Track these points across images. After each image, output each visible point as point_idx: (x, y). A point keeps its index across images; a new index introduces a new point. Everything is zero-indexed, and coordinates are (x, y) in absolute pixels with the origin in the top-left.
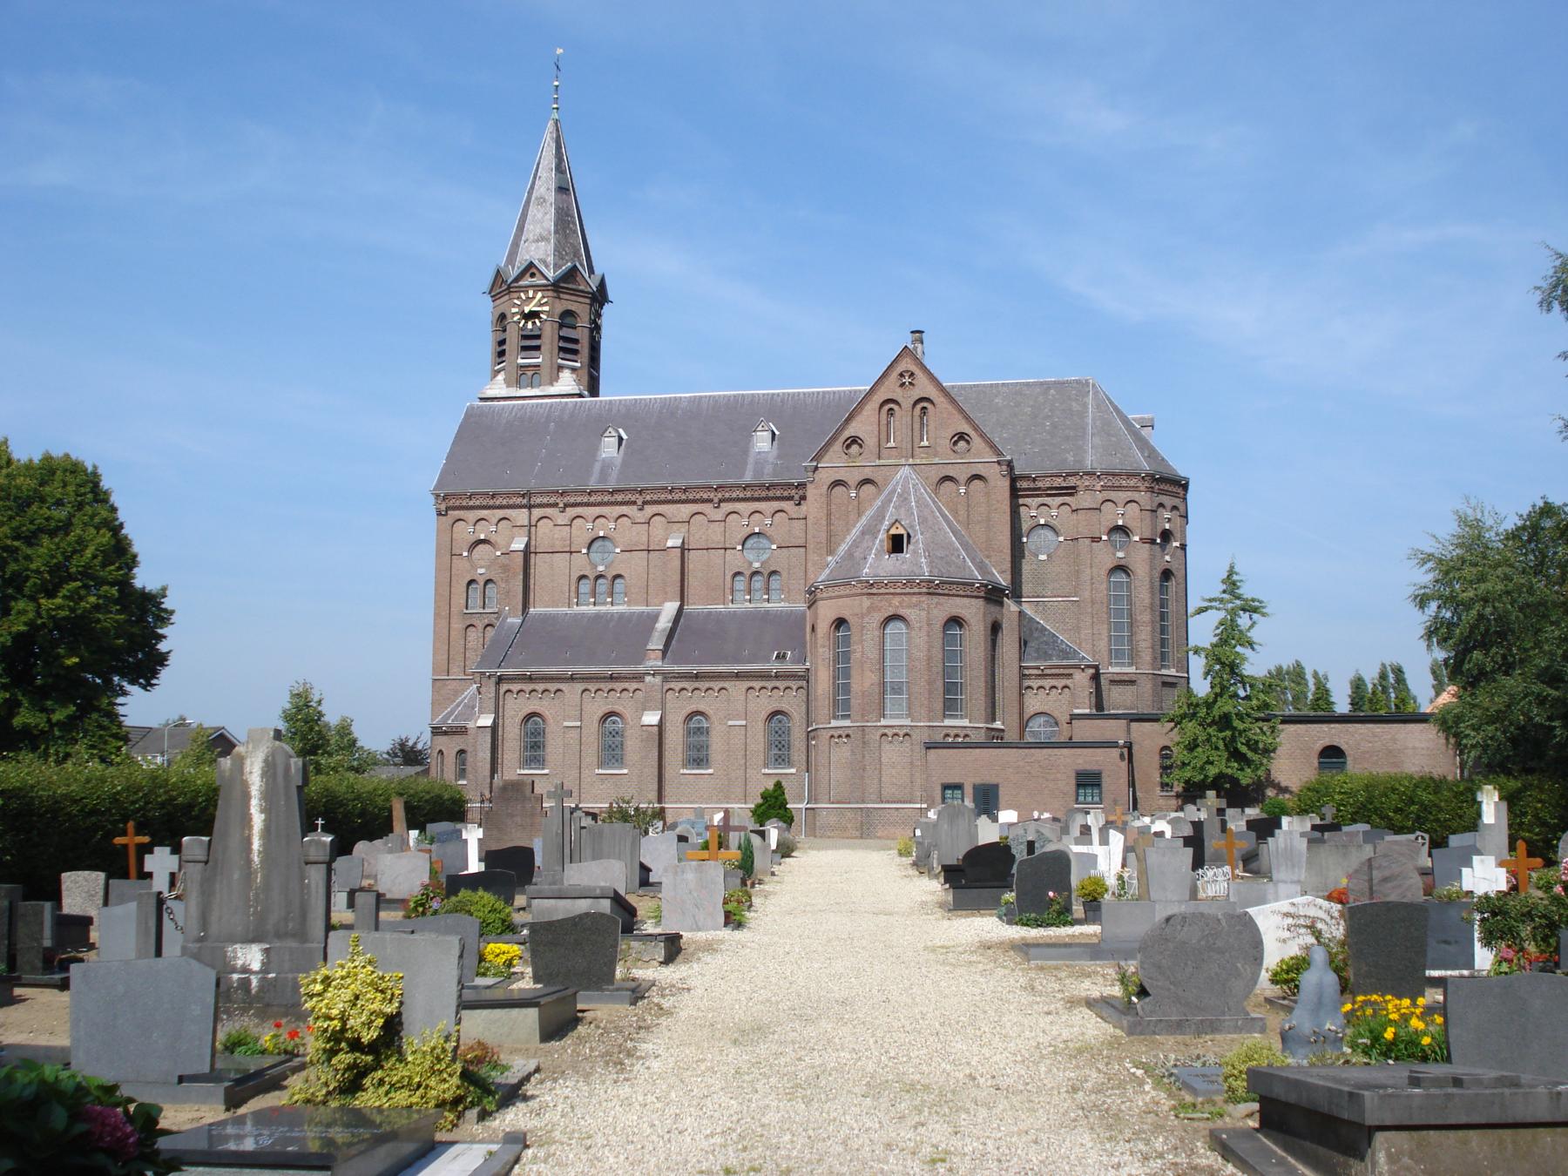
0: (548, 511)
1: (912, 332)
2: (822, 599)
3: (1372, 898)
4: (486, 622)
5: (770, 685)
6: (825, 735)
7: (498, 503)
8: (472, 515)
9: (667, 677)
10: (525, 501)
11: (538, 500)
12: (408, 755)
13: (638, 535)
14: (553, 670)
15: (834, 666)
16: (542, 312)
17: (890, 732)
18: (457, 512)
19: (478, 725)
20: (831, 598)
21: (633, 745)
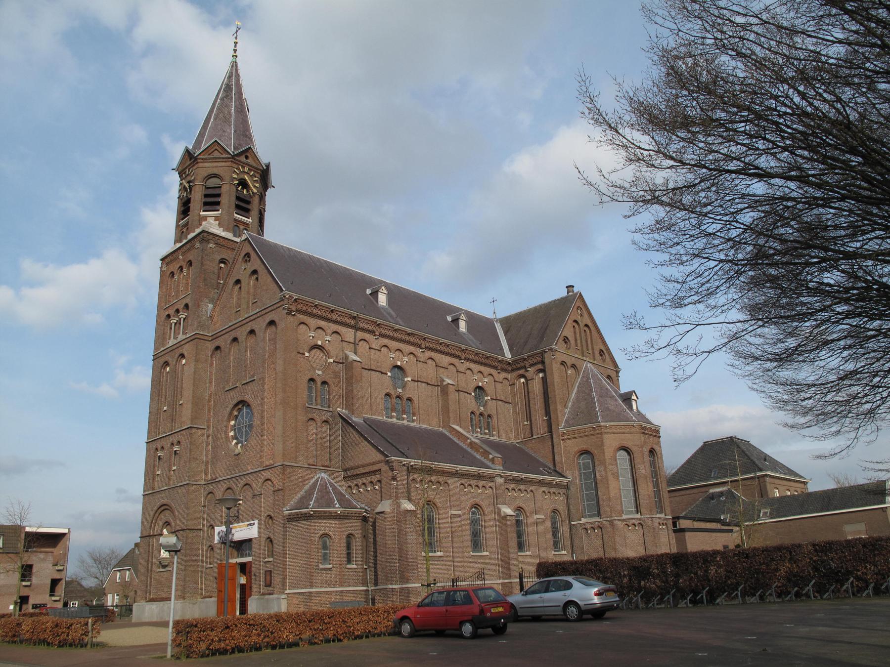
0: (367, 336)
1: (567, 287)
2: (607, 434)
3: (376, 584)
4: (324, 418)
5: (552, 490)
6: (621, 525)
7: (334, 317)
8: (314, 322)
9: (508, 480)
10: (353, 322)
11: (362, 325)
12: (738, 546)
13: (429, 372)
14: (447, 466)
15: (657, 479)
16: (252, 190)
17: (630, 523)
18: (301, 316)
19: (377, 511)
20: (614, 433)
21: (490, 532)
